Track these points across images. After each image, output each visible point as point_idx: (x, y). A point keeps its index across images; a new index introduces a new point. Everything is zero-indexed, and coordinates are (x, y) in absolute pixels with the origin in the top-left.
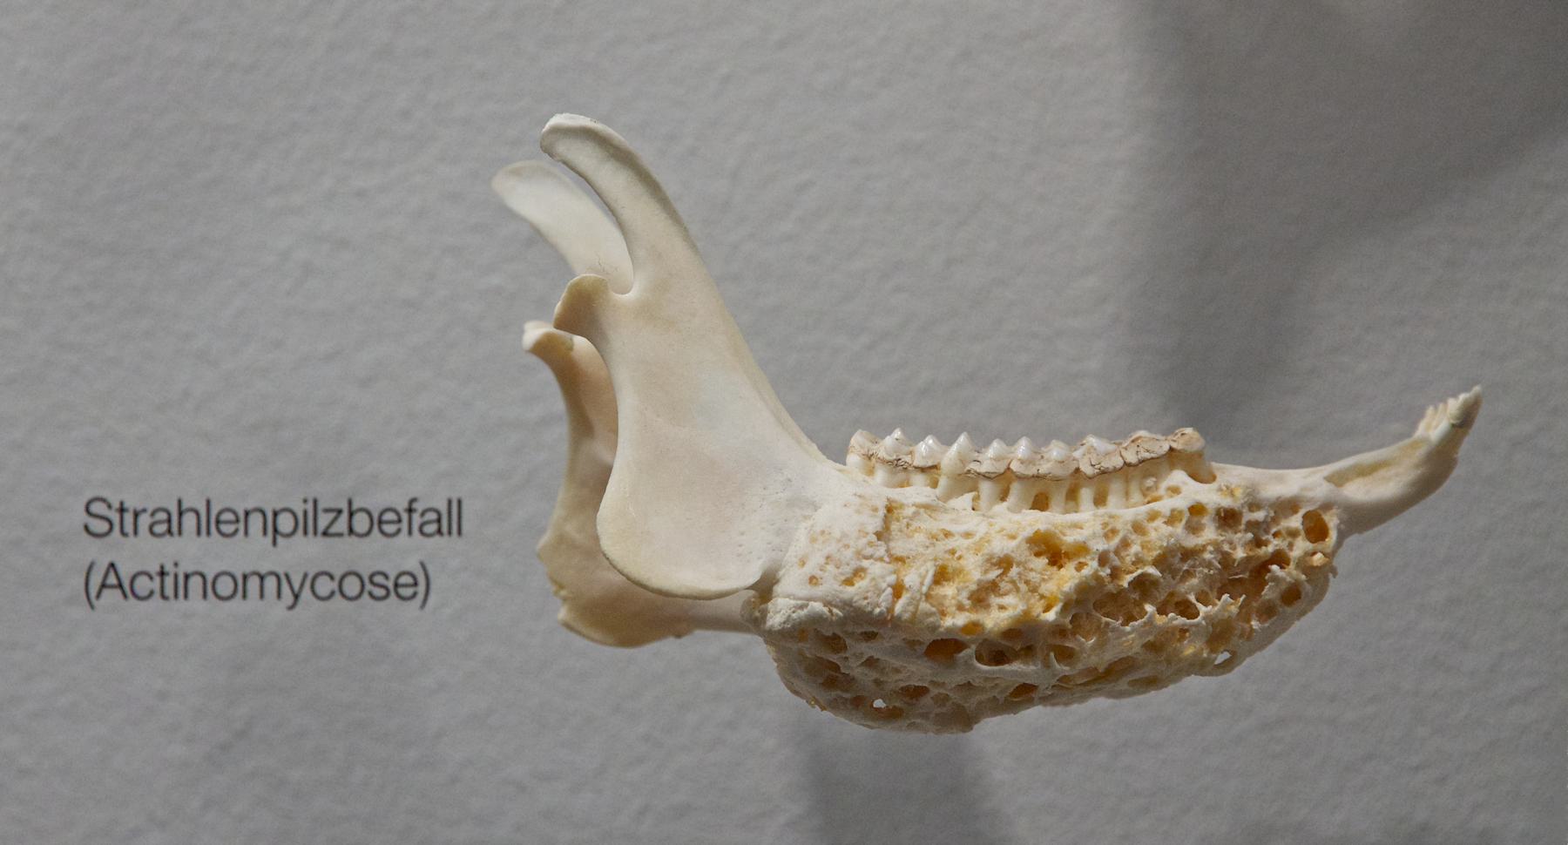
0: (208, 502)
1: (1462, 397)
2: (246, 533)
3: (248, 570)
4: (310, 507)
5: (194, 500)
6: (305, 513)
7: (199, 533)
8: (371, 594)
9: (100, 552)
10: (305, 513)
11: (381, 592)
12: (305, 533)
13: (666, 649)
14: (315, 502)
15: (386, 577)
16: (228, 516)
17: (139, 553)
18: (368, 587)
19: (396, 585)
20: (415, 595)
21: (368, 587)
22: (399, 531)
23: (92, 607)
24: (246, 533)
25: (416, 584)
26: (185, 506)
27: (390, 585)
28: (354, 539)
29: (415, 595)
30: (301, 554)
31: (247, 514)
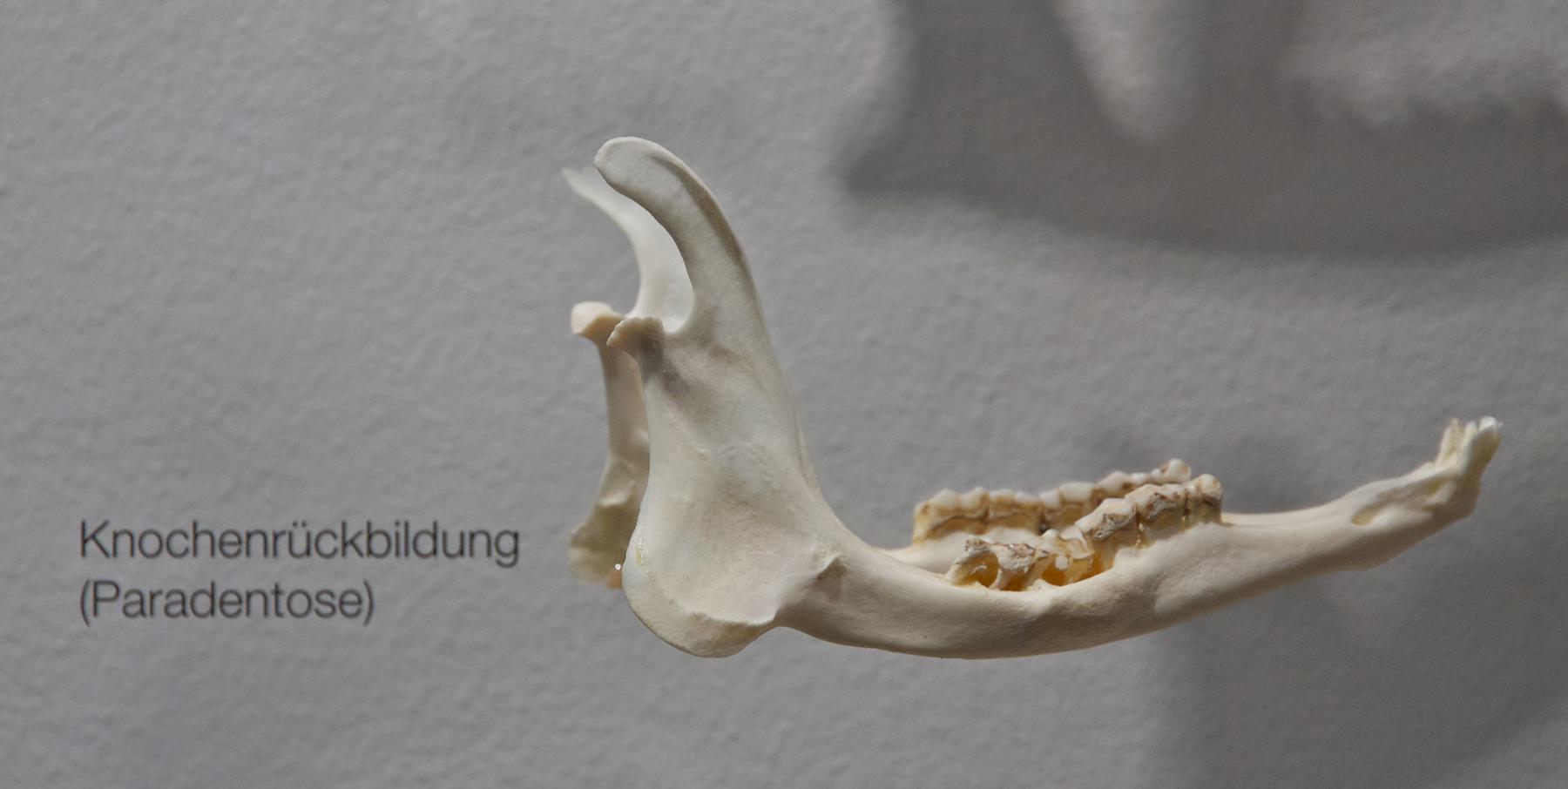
0: (344, 525)
1: (1471, 430)
2: (248, 553)
3: (251, 588)
4: (402, 530)
5: (384, 522)
6: (397, 535)
7: (266, 553)
8: (318, 612)
9: (100, 568)
10: (397, 535)
11: (327, 610)
12: (397, 553)
13: (751, 647)
14: (407, 525)
15: (332, 595)
16: (231, 538)
17: (130, 572)
18: (315, 604)
19: (342, 603)
20: (359, 612)
21: (315, 604)
22: (239, 552)
23: (87, 623)
24: (248, 553)
25: (360, 602)
26: (374, 528)
27: (336, 602)
28: (372, 559)
29: (359, 612)
30: (187, 573)
31: (249, 536)
